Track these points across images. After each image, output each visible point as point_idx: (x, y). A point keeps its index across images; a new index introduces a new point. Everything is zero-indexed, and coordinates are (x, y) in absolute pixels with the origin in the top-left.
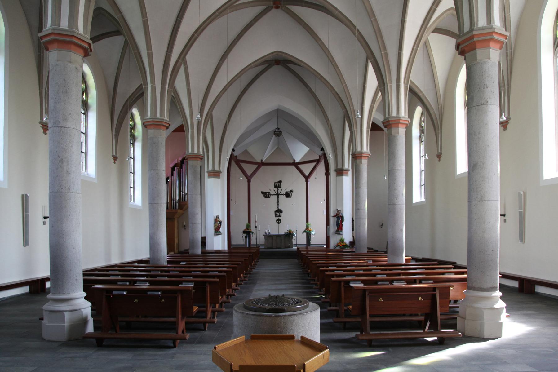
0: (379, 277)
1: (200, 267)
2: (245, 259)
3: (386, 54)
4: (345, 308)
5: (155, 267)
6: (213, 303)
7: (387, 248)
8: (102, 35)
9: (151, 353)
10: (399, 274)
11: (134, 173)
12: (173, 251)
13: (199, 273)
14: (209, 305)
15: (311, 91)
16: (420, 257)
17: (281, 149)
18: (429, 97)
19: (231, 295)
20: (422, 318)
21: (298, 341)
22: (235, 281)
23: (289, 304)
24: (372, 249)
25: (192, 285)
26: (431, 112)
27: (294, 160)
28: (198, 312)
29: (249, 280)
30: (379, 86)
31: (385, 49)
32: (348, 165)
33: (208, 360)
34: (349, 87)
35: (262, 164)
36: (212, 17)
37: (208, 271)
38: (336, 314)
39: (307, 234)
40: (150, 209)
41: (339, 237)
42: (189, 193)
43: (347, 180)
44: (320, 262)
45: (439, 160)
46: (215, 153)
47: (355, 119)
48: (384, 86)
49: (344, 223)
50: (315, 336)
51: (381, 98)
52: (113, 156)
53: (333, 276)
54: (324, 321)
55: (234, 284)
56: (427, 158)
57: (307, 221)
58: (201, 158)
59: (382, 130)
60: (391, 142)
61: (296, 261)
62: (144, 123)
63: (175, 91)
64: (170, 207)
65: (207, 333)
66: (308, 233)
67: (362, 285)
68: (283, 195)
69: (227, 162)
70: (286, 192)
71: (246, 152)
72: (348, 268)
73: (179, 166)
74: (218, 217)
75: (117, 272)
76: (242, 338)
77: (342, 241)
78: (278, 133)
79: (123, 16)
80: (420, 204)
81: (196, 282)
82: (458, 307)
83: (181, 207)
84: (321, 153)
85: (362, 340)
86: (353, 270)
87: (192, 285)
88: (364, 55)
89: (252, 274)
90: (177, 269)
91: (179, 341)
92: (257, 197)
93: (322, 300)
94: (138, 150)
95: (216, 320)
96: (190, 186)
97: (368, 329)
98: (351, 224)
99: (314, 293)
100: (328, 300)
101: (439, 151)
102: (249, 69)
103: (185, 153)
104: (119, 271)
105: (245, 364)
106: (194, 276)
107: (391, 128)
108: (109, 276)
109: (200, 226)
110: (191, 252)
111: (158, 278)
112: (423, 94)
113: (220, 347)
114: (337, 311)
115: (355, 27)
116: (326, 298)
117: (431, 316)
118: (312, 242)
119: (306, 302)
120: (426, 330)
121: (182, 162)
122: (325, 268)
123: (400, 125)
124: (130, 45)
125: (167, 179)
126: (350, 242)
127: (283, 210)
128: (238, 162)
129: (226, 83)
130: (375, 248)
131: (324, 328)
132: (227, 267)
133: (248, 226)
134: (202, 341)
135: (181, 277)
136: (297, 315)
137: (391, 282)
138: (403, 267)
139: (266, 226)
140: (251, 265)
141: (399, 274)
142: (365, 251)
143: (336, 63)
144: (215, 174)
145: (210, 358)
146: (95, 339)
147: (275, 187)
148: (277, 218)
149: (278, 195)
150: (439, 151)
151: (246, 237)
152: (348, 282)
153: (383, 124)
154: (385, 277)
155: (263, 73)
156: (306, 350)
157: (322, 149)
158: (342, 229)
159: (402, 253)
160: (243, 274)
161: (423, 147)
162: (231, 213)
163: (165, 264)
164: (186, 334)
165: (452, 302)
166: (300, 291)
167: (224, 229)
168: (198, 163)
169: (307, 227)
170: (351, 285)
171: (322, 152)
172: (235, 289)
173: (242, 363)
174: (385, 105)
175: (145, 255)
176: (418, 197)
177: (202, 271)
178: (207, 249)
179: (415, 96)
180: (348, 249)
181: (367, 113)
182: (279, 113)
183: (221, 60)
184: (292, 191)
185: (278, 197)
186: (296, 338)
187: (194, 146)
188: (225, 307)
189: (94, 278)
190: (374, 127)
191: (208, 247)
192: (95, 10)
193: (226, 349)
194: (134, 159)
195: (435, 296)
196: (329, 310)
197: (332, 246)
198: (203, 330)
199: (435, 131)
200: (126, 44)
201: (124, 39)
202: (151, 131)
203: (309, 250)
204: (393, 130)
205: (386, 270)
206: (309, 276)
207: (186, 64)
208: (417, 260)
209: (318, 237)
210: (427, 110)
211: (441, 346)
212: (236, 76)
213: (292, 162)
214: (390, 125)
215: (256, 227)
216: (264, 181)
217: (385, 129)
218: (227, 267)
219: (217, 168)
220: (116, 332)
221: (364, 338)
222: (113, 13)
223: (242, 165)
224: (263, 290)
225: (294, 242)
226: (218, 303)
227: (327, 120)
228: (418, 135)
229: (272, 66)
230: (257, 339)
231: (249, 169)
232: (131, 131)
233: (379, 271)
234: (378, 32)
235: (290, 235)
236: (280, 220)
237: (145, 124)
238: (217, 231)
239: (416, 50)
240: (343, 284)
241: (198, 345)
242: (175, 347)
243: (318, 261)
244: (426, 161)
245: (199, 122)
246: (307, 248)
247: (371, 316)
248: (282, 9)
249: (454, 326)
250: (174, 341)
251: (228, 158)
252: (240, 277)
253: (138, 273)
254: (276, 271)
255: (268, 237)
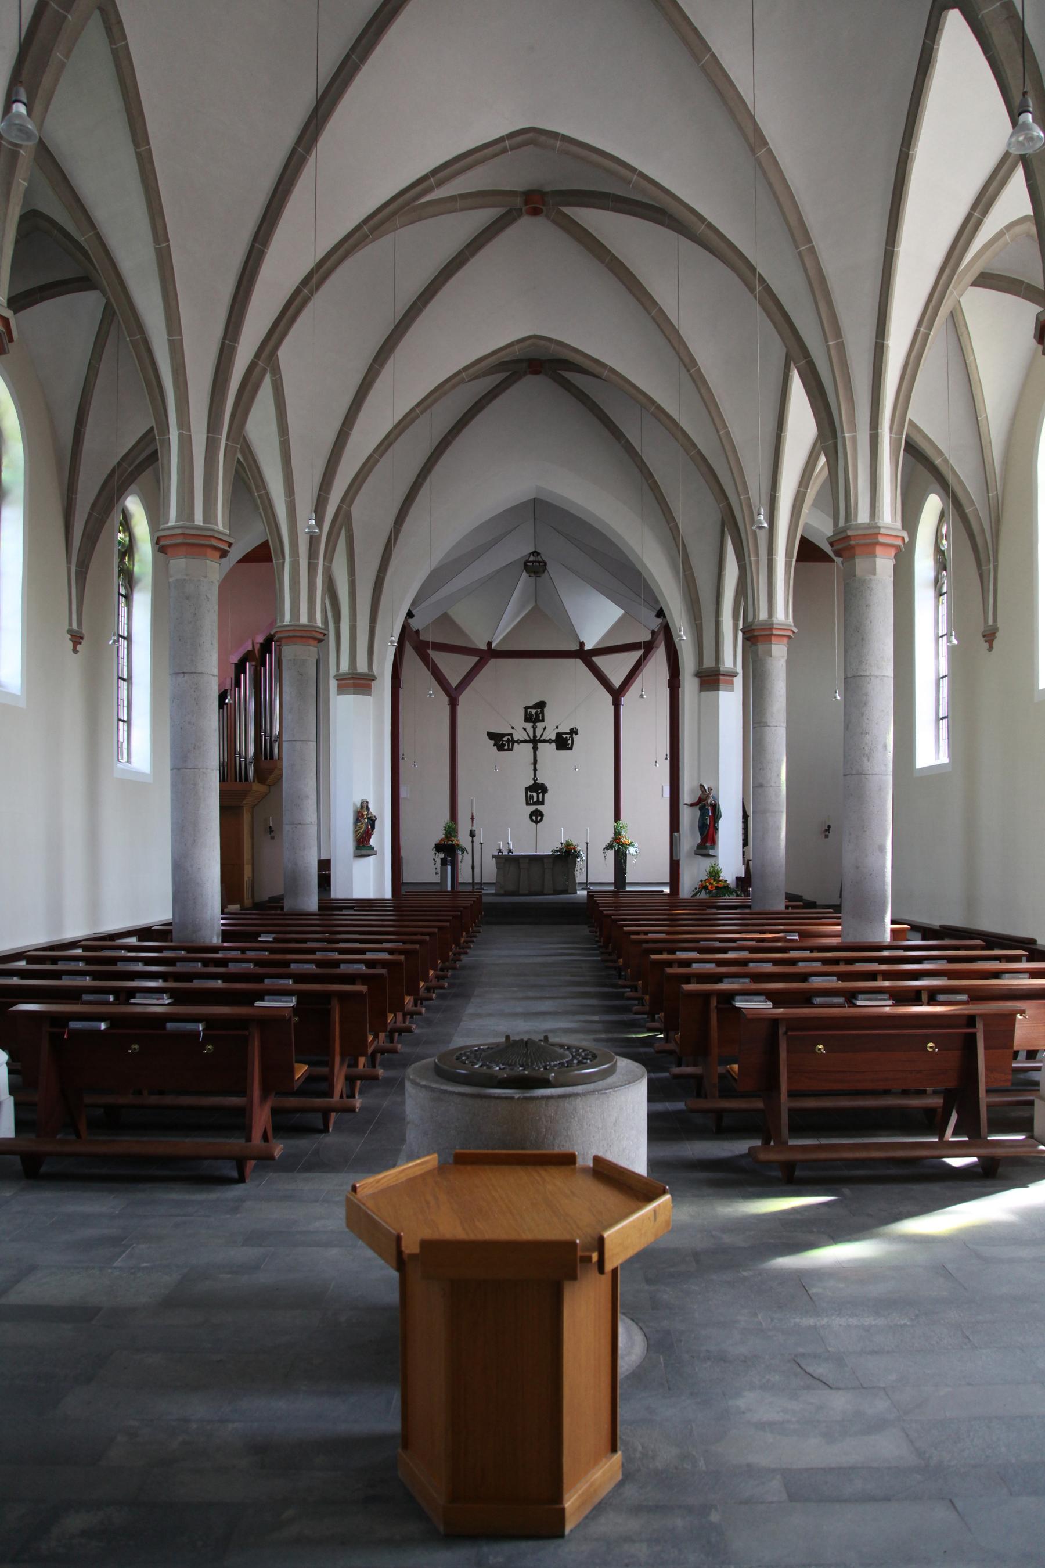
0: (817, 982)
1: (313, 951)
2: (440, 928)
3: (841, 347)
4: (721, 1070)
5: (189, 950)
6: (351, 1054)
7: (841, 897)
8: (42, 288)
9: (174, 1196)
10: (873, 976)
11: (129, 680)
12: (240, 901)
13: (312, 968)
14: (337, 1059)
15: (629, 449)
16: (936, 922)
17: (546, 611)
18: (962, 467)
19: (401, 1031)
20: (937, 1101)
21: (585, 1170)
22: (414, 991)
23: (562, 1064)
24: (798, 898)
25: (291, 1003)
26: (969, 510)
27: (582, 644)
28: (309, 1078)
29: (451, 985)
30: (821, 436)
31: (838, 334)
32: (731, 658)
33: (335, 1220)
34: (737, 437)
35: (490, 653)
36: (352, 241)
37: (336, 964)
38: (696, 1086)
39: (617, 853)
40: (174, 785)
41: (705, 864)
42: (285, 737)
43: (730, 702)
44: (651, 936)
45: (991, 648)
46: (358, 617)
47: (755, 533)
48: (835, 437)
49: (722, 824)
50: (634, 1155)
51: (826, 472)
52: (70, 631)
53: (687, 979)
54: (660, 1107)
55: (408, 999)
56: (955, 642)
57: (617, 817)
58: (320, 639)
59: (829, 559)
60: (853, 596)
61: (584, 930)
62: (157, 543)
63: (247, 449)
64: (231, 774)
65: (332, 1139)
66: (619, 849)
67: (770, 1004)
68: (550, 741)
69: (391, 651)
70: (559, 735)
71: (445, 620)
72: (731, 955)
73: (256, 659)
74: (364, 805)
75: (81, 965)
76: (431, 1160)
77: (714, 874)
78: (535, 566)
79: (99, 237)
80: (934, 774)
81: (301, 995)
82: (1038, 1069)
83: (261, 776)
84: (656, 623)
85: (768, 1163)
86: (744, 963)
87: (291, 1003)
88: (778, 350)
89: (463, 968)
90: (250, 954)
91: (253, 1162)
92: (476, 750)
93: (657, 1046)
94: (141, 616)
95: (358, 1102)
96: (287, 717)
97: (785, 1130)
98: (740, 825)
99: (634, 1026)
100: (671, 1046)
101: (990, 622)
102: (454, 386)
103: (273, 624)
104: (88, 961)
105: (436, 1236)
106: (299, 978)
107: (852, 557)
108: (57, 975)
109: (313, 830)
110: (288, 905)
111: (197, 984)
112: (946, 461)
113: (370, 1184)
114: (698, 1079)
115: (753, 269)
116: (667, 1039)
117: (962, 1095)
118: (630, 878)
119: (609, 1059)
120: (949, 1137)
121: (266, 647)
122: (665, 956)
123: (879, 550)
124: (119, 319)
125: (222, 696)
126: (738, 879)
127: (547, 785)
128: (423, 649)
129: (389, 426)
130: (808, 896)
131: (660, 1128)
132: (391, 952)
133: (451, 831)
134: (317, 1164)
135: (259, 978)
136: (584, 1094)
137: (851, 996)
138: (886, 953)
139: (502, 831)
140: (458, 945)
141: (873, 976)
142: (780, 905)
143: (699, 370)
144: (358, 683)
145: (341, 1212)
146: (17, 1159)
147: (528, 719)
148: (533, 808)
149: (535, 742)
150: (990, 622)
151: (444, 862)
152: (728, 997)
153: (832, 544)
154: (832, 983)
155: (495, 397)
156: (606, 1197)
157: (660, 614)
158: (714, 842)
159: (884, 913)
160: (435, 969)
161: (943, 609)
162: (404, 748)
163: (216, 940)
164: (273, 1141)
165: (1022, 1055)
166: (596, 1018)
167: (382, 838)
168: (310, 651)
169: (617, 833)
170: (738, 1005)
171: (660, 621)
172: (412, 1014)
173: (428, 1234)
174: (836, 492)
175: (158, 911)
176: (930, 751)
177: (319, 964)
178: (333, 896)
179: (921, 465)
180: (730, 899)
181: (788, 510)
182: (540, 511)
183: (375, 360)
184: (573, 732)
185: (535, 749)
186: (580, 1162)
187: (298, 605)
188: (384, 1067)
189: (15, 981)
190: (808, 552)
191: (338, 892)
192: (23, 218)
193: (385, 1192)
194: (129, 638)
195: (972, 1039)
196: (677, 1077)
197: (686, 889)
198: (321, 1132)
199: (981, 576)
200: (109, 314)
201: (104, 301)
202: (179, 564)
203: (622, 900)
204: (861, 564)
205: (836, 962)
206: (620, 977)
207: (276, 371)
208: (926, 932)
209: (649, 866)
210: (956, 506)
211: (988, 1183)
212: (418, 405)
213: (575, 647)
214: (852, 548)
215: (472, 834)
216: (496, 701)
217: (835, 558)
218: (391, 952)
219: (362, 667)
220: (79, 1136)
221: (773, 1156)
222: (70, 228)
223: (433, 654)
224: (490, 1015)
225: (580, 878)
226: (364, 1054)
227: (674, 530)
228: (931, 574)
229: (520, 378)
230: (472, 1163)
231: (454, 668)
232: (122, 561)
233: (817, 966)
234: (818, 286)
235: (567, 856)
236: (542, 815)
237: (162, 543)
238: (363, 845)
239: (927, 336)
240: (714, 1002)
241: (307, 1175)
242: (241, 1179)
243: (646, 933)
244: (952, 651)
245: (313, 540)
246: (615, 893)
247: (792, 1094)
248: (548, 217)
249: (1025, 1125)
250: (241, 1163)
251: (395, 638)
252: (426, 979)
253: (140, 967)
254: (527, 961)
255: (507, 861)
